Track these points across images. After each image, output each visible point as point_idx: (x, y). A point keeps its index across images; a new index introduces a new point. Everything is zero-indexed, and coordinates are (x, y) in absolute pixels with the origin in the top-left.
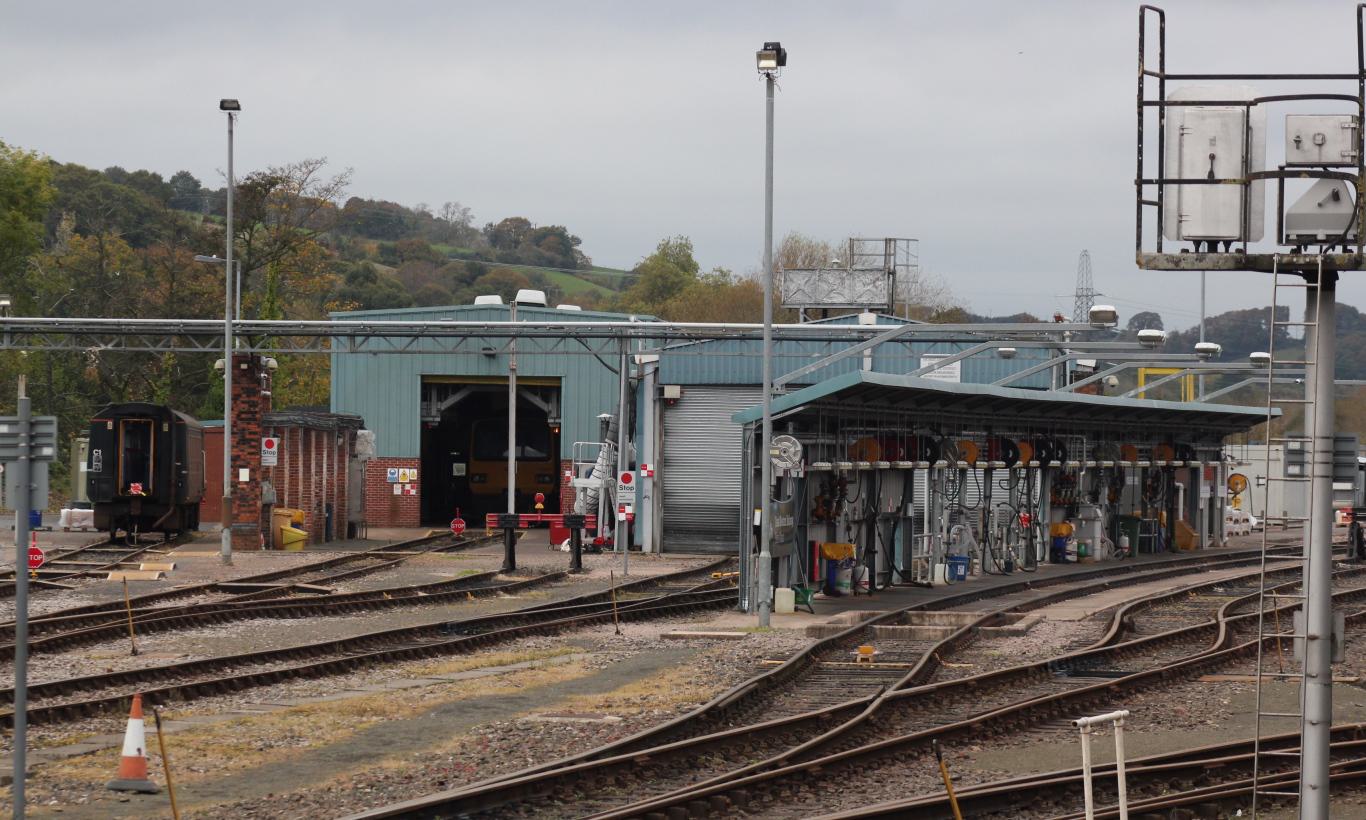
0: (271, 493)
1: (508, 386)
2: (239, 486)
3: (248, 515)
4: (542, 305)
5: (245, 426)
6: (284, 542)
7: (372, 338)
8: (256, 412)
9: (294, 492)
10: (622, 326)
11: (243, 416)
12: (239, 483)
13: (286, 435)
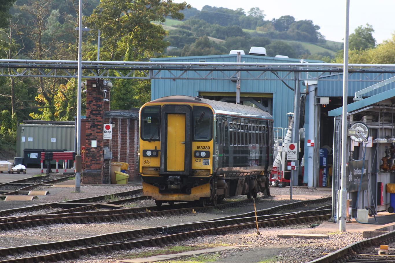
0: (109, 153)
1: (235, 97)
2: (91, 150)
3: (96, 165)
4: (264, 55)
5: (94, 117)
6: (117, 179)
7: (162, 71)
8: (101, 110)
9: (124, 153)
10: (297, 65)
11: (94, 112)
12: (91, 148)
13: (119, 123)
